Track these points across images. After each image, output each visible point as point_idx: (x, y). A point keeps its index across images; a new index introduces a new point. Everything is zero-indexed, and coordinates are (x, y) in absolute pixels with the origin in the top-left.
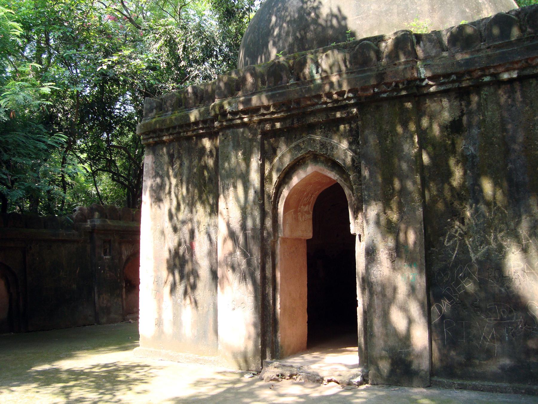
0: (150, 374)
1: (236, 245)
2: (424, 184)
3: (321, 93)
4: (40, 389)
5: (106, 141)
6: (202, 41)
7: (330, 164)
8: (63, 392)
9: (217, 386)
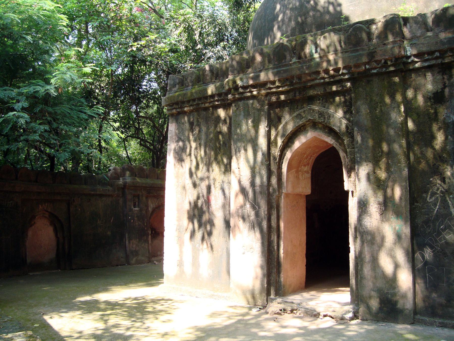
0: (173, 307)
1: (246, 199)
2: (409, 147)
3: (320, 70)
4: (83, 316)
5: (134, 113)
6: (215, 27)
7: (327, 130)
8: (102, 319)
9: (229, 318)
